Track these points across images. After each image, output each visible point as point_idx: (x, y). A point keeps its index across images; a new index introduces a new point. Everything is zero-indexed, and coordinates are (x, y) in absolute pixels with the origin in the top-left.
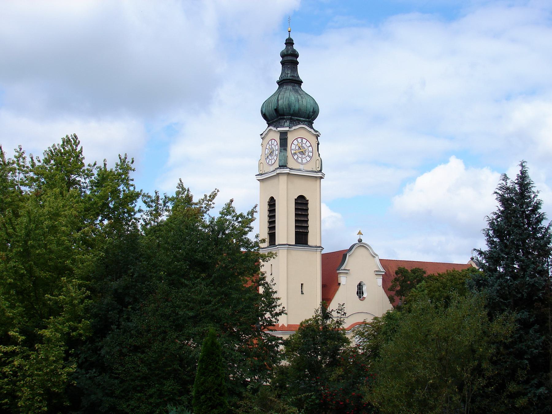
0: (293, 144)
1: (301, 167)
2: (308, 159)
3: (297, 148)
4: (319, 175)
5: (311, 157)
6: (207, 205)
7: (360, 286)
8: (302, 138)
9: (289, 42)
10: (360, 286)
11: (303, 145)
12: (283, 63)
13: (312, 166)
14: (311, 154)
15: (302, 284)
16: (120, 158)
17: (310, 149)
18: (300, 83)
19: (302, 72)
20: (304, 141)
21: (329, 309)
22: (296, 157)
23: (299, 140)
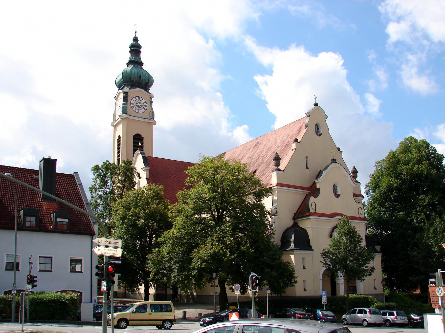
0: (133, 101)
1: (139, 115)
2: (144, 111)
3: (135, 103)
4: (151, 121)
5: (146, 110)
6: (133, 244)
7: (335, 188)
8: (139, 97)
9: (136, 39)
10: (335, 188)
11: (140, 101)
12: (130, 52)
13: (146, 115)
14: (146, 108)
15: (304, 281)
16: (323, 263)
17: (145, 104)
18: (141, 64)
19: (144, 57)
20: (141, 99)
21: (192, 255)
22: (134, 109)
23: (137, 98)
